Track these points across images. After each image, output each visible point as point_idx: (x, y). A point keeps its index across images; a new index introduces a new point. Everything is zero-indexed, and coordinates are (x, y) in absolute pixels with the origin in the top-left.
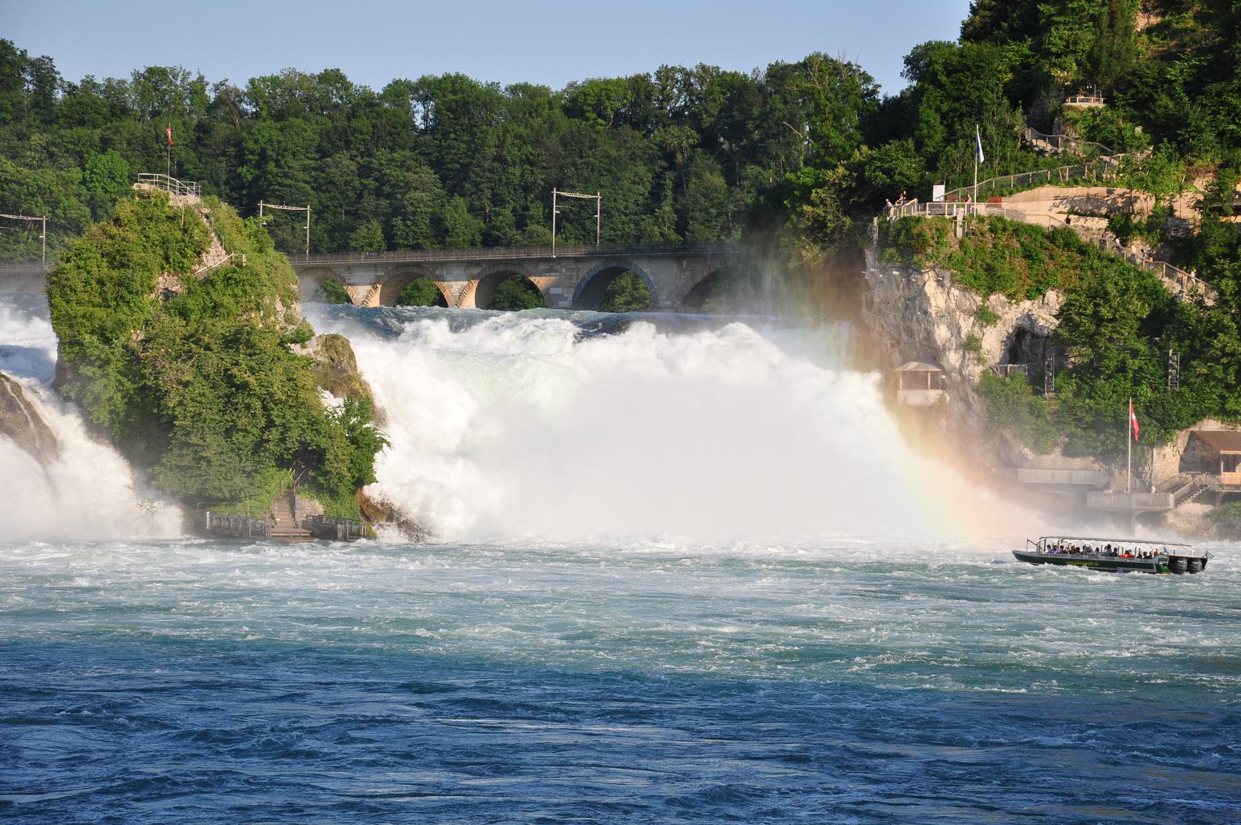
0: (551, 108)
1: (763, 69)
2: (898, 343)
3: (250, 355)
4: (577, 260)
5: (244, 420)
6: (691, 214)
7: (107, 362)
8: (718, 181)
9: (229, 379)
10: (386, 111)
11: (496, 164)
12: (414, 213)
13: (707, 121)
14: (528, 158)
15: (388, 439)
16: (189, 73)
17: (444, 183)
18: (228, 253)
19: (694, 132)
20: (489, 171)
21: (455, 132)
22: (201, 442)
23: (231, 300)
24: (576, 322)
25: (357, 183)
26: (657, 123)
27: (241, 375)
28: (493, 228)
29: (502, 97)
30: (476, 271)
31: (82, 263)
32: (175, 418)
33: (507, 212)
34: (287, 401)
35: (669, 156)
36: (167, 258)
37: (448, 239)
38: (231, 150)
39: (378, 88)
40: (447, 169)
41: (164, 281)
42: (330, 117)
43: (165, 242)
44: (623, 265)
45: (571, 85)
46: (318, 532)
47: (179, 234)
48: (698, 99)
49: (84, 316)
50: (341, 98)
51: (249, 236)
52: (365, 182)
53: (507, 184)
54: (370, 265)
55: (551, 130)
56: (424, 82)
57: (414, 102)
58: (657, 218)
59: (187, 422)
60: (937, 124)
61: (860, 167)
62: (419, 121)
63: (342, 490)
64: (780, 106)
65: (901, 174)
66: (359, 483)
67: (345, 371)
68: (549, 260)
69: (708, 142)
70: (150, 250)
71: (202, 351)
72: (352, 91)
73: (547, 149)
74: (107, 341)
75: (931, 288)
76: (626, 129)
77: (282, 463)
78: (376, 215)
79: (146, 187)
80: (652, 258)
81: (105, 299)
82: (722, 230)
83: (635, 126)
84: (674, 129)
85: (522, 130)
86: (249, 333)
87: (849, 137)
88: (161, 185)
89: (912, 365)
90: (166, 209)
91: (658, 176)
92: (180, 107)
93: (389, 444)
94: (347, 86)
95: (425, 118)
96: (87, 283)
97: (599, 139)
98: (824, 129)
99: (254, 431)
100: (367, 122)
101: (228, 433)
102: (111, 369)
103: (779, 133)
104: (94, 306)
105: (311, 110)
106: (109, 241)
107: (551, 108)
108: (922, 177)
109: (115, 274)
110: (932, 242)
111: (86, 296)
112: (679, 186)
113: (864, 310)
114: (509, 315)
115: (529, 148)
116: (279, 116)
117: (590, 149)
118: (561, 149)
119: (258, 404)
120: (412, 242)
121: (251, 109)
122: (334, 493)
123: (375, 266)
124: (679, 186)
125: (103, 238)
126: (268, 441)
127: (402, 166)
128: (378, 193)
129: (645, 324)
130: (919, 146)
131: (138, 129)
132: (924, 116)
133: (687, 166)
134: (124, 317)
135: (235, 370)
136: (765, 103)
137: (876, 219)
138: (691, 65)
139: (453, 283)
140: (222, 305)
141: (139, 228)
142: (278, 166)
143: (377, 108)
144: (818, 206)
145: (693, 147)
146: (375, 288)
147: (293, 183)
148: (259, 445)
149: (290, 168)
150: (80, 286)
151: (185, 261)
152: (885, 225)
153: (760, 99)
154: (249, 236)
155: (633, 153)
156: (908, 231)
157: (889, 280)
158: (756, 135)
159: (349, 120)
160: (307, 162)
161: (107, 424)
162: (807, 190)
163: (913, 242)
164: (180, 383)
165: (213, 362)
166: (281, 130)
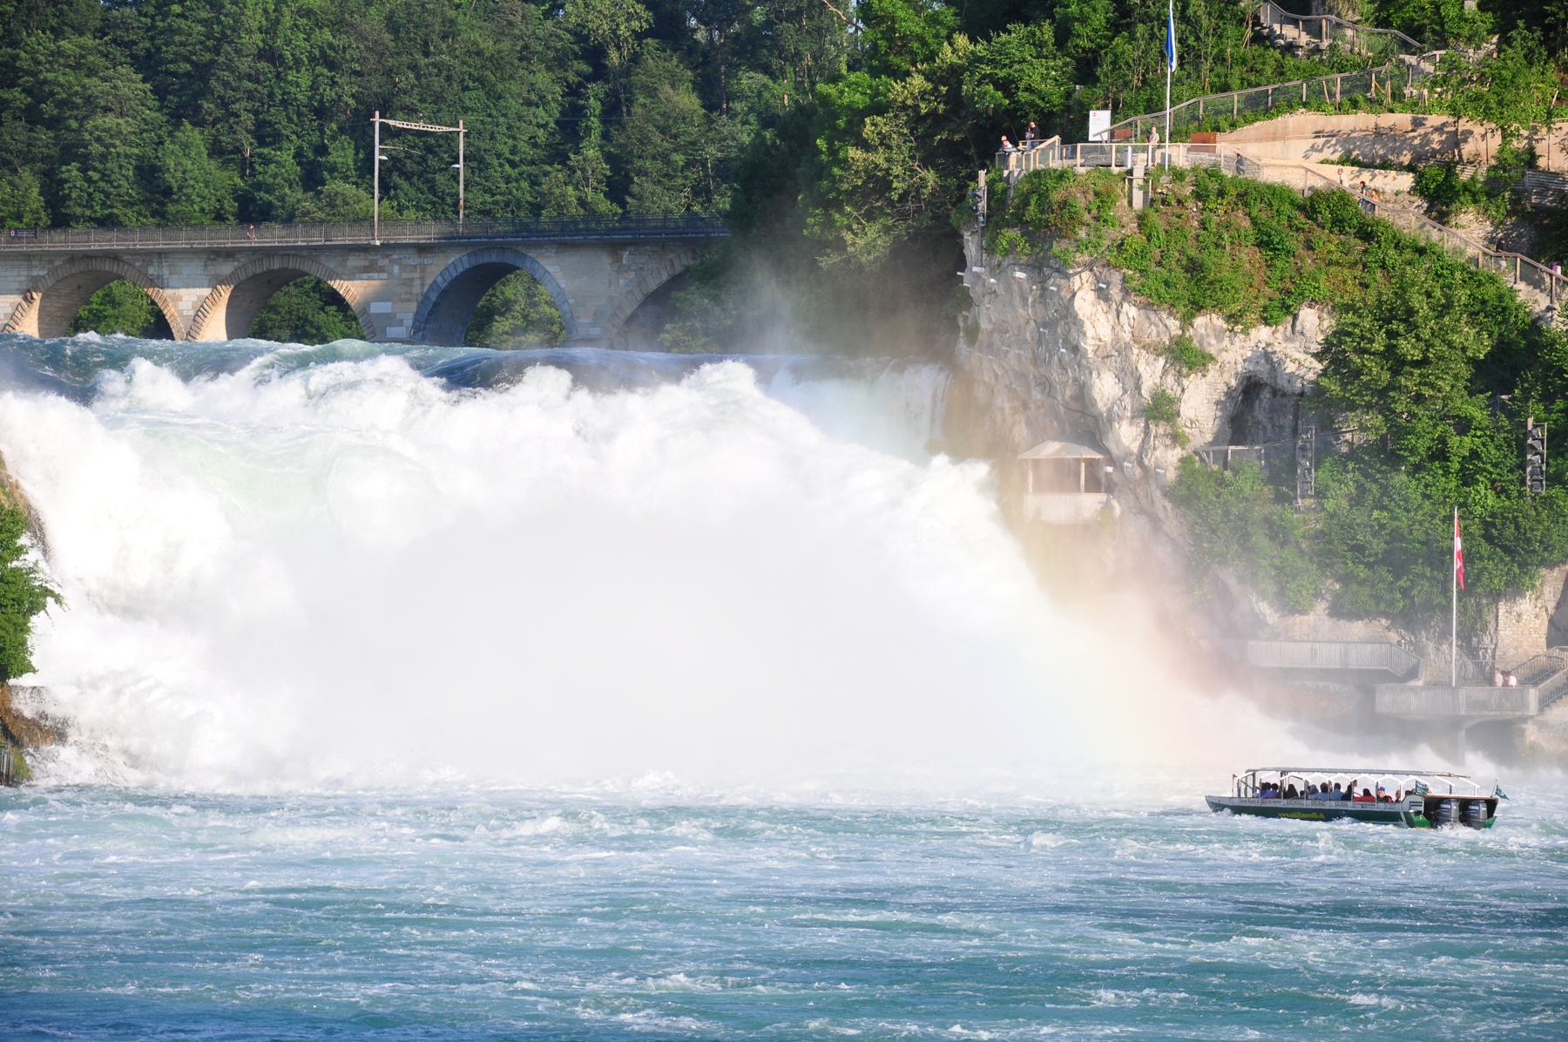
2: (1025, 406)
4: (422, 249)
6: (638, 163)
8: (687, 100)
11: (262, 65)
12: (103, 158)
15: (57, 591)
17: (162, 100)
19: (640, 8)
20: (249, 77)
28: (259, 186)
30: (226, 268)
33: (286, 156)
35: (595, 54)
37: (171, 208)
40: (168, 73)
44: (509, 259)
53: (284, 103)
61: (953, 75)
65: (1029, 89)
68: (366, 249)
73: (362, 37)
75: (1085, 303)
78: (28, 159)
82: (696, 192)
91: (574, 91)
97: (460, 19)
108: (1068, 95)
110: (1087, 217)
112: (613, 111)
115: (327, 35)
117: (444, 37)
118: (387, 37)
120: (100, 212)
123: (28, 257)
124: (613, 111)
127: (77, 67)
128: (32, 116)
130: (1063, 35)
133: (627, 73)
139: (183, 292)
145: (639, 36)
152: (1000, 186)
155: (526, 47)
157: (1008, 289)
162: (858, 116)
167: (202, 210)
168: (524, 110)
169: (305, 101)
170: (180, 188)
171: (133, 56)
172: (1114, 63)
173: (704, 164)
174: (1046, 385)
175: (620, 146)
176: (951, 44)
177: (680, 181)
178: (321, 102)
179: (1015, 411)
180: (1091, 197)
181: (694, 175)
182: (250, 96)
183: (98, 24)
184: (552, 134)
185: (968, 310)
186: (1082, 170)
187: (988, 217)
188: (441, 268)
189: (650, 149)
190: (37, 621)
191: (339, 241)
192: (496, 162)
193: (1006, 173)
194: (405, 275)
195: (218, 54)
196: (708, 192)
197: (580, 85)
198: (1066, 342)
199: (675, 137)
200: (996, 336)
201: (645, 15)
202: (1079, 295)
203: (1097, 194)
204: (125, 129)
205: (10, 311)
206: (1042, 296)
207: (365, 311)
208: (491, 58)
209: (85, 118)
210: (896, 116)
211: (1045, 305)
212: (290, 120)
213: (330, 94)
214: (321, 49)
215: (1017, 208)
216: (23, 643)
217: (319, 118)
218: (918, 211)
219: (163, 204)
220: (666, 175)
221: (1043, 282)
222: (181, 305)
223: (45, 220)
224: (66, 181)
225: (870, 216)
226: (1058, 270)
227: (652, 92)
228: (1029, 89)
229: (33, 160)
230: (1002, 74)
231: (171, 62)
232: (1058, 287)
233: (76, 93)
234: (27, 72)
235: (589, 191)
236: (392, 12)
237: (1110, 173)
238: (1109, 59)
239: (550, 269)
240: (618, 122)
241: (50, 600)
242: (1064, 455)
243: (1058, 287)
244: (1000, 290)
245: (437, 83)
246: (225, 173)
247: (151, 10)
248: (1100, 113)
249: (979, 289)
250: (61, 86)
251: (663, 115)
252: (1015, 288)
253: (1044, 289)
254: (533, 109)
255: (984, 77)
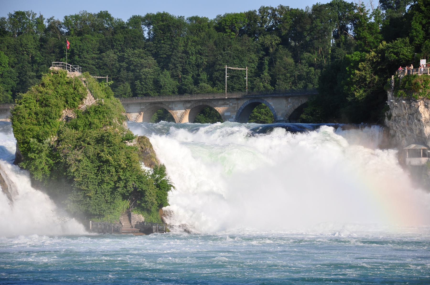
0: (209, 28)
1: (311, 7)
2: (405, 135)
3: (109, 147)
4: (237, 99)
5: (107, 178)
7: (41, 151)
8: (290, 60)
9: (99, 157)
10: (130, 30)
11: (184, 55)
12: (145, 79)
13: (284, 32)
14: (199, 52)
15: (173, 185)
16: (35, 14)
17: (159, 64)
18: (95, 99)
19: (278, 38)
21: (164, 40)
22: (86, 189)
23: (98, 121)
24: (248, 127)
25: (117, 65)
26: (260, 34)
27: (105, 156)
28: (183, 85)
29: (186, 23)
30: (189, 105)
31: (27, 105)
32: (74, 177)
33: (190, 77)
34: (126, 168)
35: (266, 50)
36: (67, 102)
37: (162, 91)
38: (57, 50)
39: (125, 19)
40: (160, 57)
41: (65, 112)
42: (104, 34)
43: (65, 94)
44: (260, 101)
45: (218, 16)
46: (143, 230)
47: (72, 90)
48: (279, 22)
49: (29, 130)
50: (108, 24)
51: (102, 90)
52: (122, 64)
53: (189, 64)
54: (138, 103)
55: (210, 38)
56: (148, 17)
57: (143, 26)
58: (262, 79)
59: (81, 179)
60: (420, 30)
61: (382, 52)
62: (146, 35)
63: (153, 209)
64: (319, 24)
65: (403, 55)
66: (161, 206)
67: (148, 153)
68: (224, 99)
69: (284, 42)
70: (59, 98)
71: (86, 145)
72: (114, 21)
73: (208, 47)
74: (40, 141)
75: (422, 109)
76: (246, 36)
77: (124, 197)
78: (127, 80)
79: (56, 68)
80: (273, 97)
81: (39, 122)
82: (293, 83)
83: (250, 35)
84: (268, 37)
85: (195, 38)
86: (108, 136)
87: (376, 38)
88: (63, 67)
89: (413, 146)
90: (66, 79)
91: (261, 59)
92: (32, 30)
93: (174, 187)
94: (111, 19)
95: (149, 33)
96: (30, 114)
97: (232, 42)
98: (364, 34)
99: (111, 182)
100: (122, 36)
101: (99, 184)
102: (43, 154)
103: (319, 37)
104: (33, 125)
105: (94, 30)
106: (40, 94)
107: (209, 28)
108: (413, 56)
109: (43, 109)
110: (422, 87)
111: (29, 120)
112: (271, 63)
113: (386, 120)
114: (219, 124)
115: (200, 47)
116: (79, 34)
117: (228, 46)
118: (214, 47)
119: (114, 170)
120: (144, 92)
121: (65, 31)
122: (149, 211)
123: (140, 104)
124: (271, 63)
125: (37, 93)
126: (119, 187)
127: (139, 57)
128: (128, 69)
129: (376, 127)
130: (412, 40)
131: (12, 41)
132: (414, 27)
133: (274, 53)
134: (48, 130)
135: (102, 154)
136: (312, 23)
137: (393, 76)
138: (275, 6)
139: (178, 111)
140: (94, 123)
141: (53, 88)
142: (80, 57)
143: (127, 29)
144: (362, 71)
145: (278, 45)
146: (140, 114)
147: (87, 65)
148: (115, 188)
149: (85, 58)
150: (27, 116)
151: (76, 103)
152: (398, 79)
153: (309, 21)
154: (102, 90)
155: (249, 48)
156: (410, 82)
157: (401, 105)
158: (308, 38)
159: (113, 35)
160: (94, 55)
161: (41, 180)
162: (356, 63)
163: (412, 87)
164: (77, 160)
165: (92, 150)
166: (81, 40)
167: (169, 91)
168: (249, 64)
169: (194, 63)
170: (164, 86)
171: (152, 54)
172: (426, 47)
173: (294, 76)
174: (411, 130)
175: (273, 72)
176: (382, 44)
177: (289, 81)
178: (198, 63)
179: (402, 137)
180: (423, 82)
181: (293, 79)
182: (181, 62)
183: (143, 46)
184: (256, 70)
185: (388, 111)
186: (420, 75)
187: (395, 87)
188: (242, 104)
189: (281, 73)
190: (169, 193)
191: (217, 98)
192: (242, 77)
193: (399, 76)
194: (233, 106)
195: (173, 52)
196: (296, 83)
197: (263, 57)
198: (417, 119)
199: (287, 70)
200: (397, 117)
201: (279, 39)
202: (420, 106)
203: (424, 81)
204: (150, 71)
205: (136, 117)
206: (410, 107)
207: (223, 115)
208: (240, 51)
209: (141, 69)
210: (367, 62)
211: (411, 110)
212: (191, 68)
213: (200, 61)
214: (198, 50)
215: (403, 85)
216: (166, 198)
217: (198, 67)
218: (373, 86)
219: (160, 90)
220: (285, 79)
221: (410, 104)
222: (178, 115)
223: (131, 95)
224: (136, 85)
225: (360, 88)
226: (414, 100)
227: (281, 59)
228: (403, 55)
229: (128, 80)
230: (395, 51)
231: (161, 55)
232: (414, 105)
233: (138, 63)
234: (127, 58)
235: (266, 84)
236: (215, 40)
237: (428, 75)
238: (425, 46)
239: (270, 103)
240: (273, 66)
241: (172, 188)
242: (416, 148)
243: (414, 105)
244: (398, 106)
245: (227, 58)
246: (175, 82)
247: (156, 42)
248: (423, 60)
249: (392, 106)
250: (135, 61)
251: (284, 64)
252: (402, 105)
253: (410, 105)
254: (251, 64)
255: (391, 52)
